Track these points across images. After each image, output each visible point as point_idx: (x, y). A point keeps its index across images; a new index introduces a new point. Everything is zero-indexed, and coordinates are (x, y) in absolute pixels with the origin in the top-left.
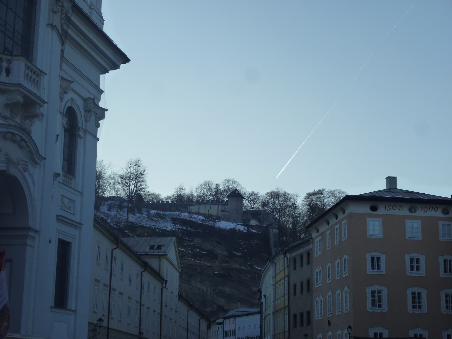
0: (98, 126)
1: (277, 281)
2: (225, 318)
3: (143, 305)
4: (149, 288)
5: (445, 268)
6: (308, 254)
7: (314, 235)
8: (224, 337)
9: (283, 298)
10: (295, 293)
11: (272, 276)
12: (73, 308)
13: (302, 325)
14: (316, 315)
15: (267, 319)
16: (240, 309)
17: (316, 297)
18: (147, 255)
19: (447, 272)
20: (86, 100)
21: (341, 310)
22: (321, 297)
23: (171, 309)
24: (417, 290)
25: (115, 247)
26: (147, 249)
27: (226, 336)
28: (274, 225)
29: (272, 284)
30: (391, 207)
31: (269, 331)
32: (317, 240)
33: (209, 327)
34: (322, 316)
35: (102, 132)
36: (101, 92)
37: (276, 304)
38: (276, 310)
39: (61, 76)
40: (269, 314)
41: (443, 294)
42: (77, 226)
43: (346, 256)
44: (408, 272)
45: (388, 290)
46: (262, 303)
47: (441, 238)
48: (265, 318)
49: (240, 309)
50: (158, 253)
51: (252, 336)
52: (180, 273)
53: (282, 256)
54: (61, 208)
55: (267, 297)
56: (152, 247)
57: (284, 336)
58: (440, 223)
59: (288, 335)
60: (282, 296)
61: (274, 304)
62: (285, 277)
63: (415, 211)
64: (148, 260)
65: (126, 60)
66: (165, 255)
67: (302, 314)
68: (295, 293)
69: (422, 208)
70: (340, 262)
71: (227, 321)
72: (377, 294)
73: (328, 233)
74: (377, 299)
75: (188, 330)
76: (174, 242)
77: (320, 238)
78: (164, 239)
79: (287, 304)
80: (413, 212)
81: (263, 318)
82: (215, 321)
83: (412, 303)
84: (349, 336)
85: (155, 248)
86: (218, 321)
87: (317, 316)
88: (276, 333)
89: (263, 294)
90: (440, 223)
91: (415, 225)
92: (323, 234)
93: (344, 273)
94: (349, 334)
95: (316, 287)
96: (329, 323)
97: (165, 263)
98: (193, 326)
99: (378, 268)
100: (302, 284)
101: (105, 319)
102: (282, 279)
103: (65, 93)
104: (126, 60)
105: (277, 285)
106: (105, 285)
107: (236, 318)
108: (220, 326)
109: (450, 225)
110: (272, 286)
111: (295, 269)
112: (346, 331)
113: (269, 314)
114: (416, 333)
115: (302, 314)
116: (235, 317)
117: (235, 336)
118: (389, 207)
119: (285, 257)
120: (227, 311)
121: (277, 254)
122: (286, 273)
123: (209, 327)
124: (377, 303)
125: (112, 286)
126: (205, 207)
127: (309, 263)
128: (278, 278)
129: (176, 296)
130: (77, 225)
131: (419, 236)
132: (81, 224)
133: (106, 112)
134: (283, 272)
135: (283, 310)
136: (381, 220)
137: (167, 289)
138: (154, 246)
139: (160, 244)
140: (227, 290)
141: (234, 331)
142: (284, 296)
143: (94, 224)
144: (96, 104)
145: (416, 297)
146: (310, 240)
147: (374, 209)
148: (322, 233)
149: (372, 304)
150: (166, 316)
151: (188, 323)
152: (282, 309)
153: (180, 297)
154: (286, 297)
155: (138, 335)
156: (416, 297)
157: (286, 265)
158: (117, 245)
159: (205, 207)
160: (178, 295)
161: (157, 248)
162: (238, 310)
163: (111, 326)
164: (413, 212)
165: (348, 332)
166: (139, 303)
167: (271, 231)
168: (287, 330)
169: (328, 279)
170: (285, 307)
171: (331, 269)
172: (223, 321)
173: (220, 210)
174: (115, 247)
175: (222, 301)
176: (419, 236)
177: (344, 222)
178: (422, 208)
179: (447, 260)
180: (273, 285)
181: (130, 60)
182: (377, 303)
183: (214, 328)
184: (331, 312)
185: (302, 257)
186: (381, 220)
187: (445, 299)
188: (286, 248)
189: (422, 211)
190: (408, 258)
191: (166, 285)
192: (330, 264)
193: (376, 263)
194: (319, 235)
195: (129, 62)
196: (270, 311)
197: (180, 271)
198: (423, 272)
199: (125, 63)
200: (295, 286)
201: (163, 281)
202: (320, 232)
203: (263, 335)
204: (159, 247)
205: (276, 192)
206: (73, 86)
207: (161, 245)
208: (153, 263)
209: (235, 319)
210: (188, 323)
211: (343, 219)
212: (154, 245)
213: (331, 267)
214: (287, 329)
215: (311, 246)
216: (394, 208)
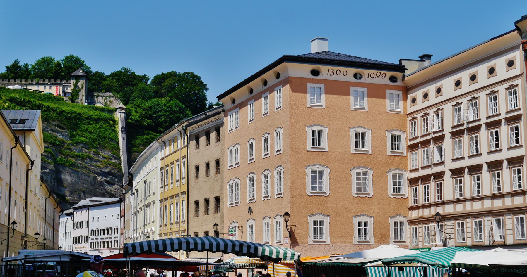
2: (75, 209)
5: (356, 142)
8: (74, 228)
10: (197, 177)
19: (359, 147)
27: (77, 228)
29: (160, 167)
51: (108, 228)
68: (197, 177)
80: (358, 78)
83: (312, 178)
85: (17, 122)
100: (208, 165)
108: (69, 218)
114: (315, 219)
117: (88, 228)
118: (332, 71)
138: (17, 120)
141: (87, 222)
149: (314, 236)
164: (358, 78)
187: (392, 180)
189: (368, 77)
191: (32, 167)
204: (23, 121)
212: (15, 118)
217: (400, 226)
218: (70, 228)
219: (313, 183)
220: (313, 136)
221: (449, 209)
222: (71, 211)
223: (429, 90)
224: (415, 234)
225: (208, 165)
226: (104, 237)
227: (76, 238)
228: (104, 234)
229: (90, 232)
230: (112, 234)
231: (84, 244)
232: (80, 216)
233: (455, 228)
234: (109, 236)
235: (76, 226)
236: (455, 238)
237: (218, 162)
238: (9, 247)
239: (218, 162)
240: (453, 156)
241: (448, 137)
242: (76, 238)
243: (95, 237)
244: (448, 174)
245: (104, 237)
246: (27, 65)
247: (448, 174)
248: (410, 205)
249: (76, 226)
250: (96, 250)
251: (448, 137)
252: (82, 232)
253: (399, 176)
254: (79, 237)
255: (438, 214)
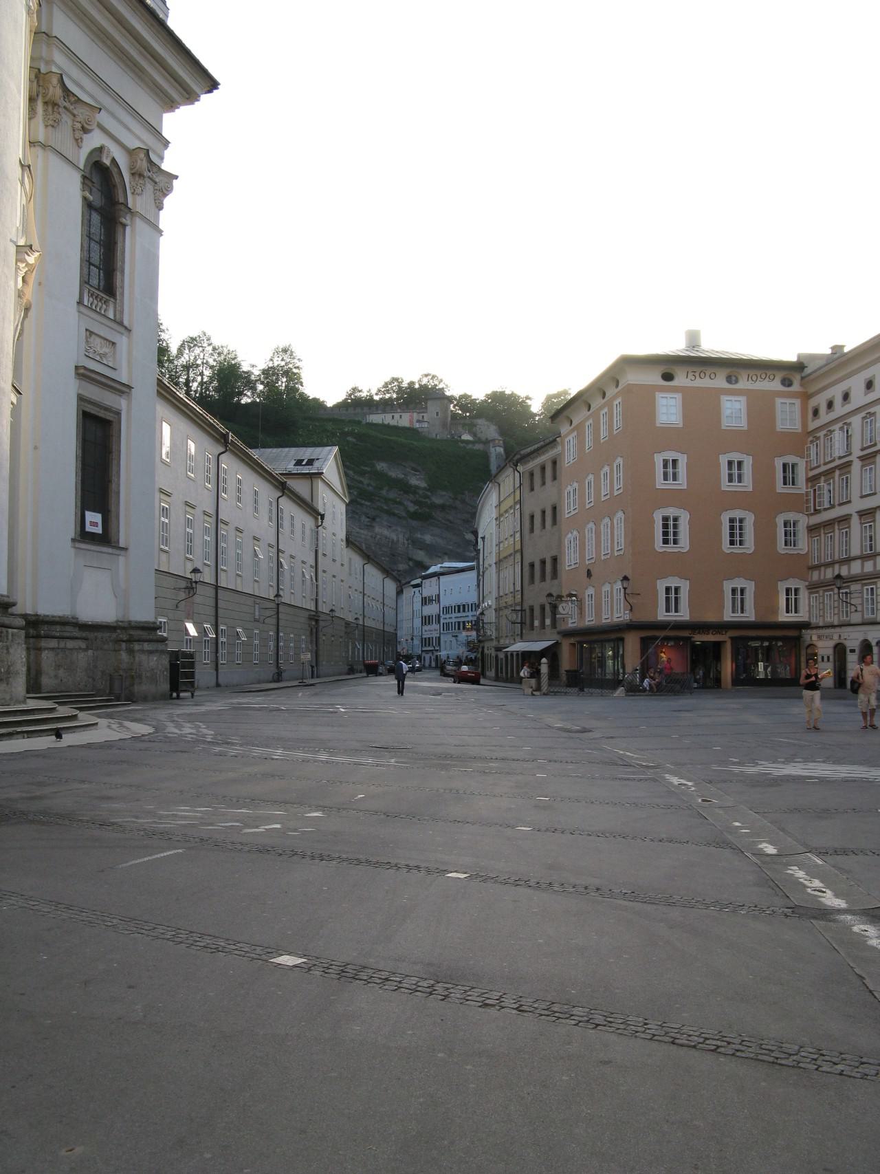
0: (160, 207)
1: (502, 512)
3: (283, 552)
4: (292, 525)
5: (785, 478)
6: (554, 463)
7: (565, 429)
9: (512, 539)
10: (532, 530)
11: (494, 505)
12: (122, 545)
13: (543, 578)
14: (567, 561)
15: (487, 573)
16: (447, 564)
17: (567, 534)
18: (290, 475)
20: (131, 153)
21: (609, 551)
22: (575, 533)
23: (334, 560)
24: (737, 514)
25: (222, 450)
26: (291, 467)
28: (497, 441)
29: (495, 517)
30: (697, 375)
31: (490, 592)
32: (570, 437)
33: (400, 592)
34: (576, 563)
35: (166, 219)
36: (166, 143)
37: (501, 549)
38: (501, 557)
39: (98, 122)
40: (490, 566)
41: (780, 520)
42: (123, 392)
43: (620, 460)
44: (725, 485)
45: (690, 515)
46: (479, 550)
47: (780, 427)
48: (483, 573)
49: (447, 564)
50: (308, 472)
52: (347, 505)
53: (509, 471)
54: (86, 355)
55: (486, 540)
56: (299, 463)
57: (515, 597)
58: (779, 401)
59: (520, 596)
60: (511, 536)
61: (497, 548)
62: (515, 503)
63: (737, 382)
64: (291, 483)
65: (213, 85)
66: (319, 474)
67: (543, 562)
68: (532, 530)
69: (749, 375)
70: (608, 472)
71: (427, 582)
72: (671, 523)
73: (588, 423)
74: (671, 530)
75: (384, 604)
76: (335, 455)
77: (575, 433)
78: (319, 449)
79: (518, 547)
80: (734, 382)
81: (481, 573)
82: (409, 582)
83: (730, 537)
84: (625, 593)
85: (304, 463)
86: (414, 582)
87: (570, 560)
88: (501, 594)
89: (480, 535)
90: (779, 401)
91: (737, 406)
92: (580, 428)
93: (616, 488)
94: (625, 589)
95: (567, 516)
96: (589, 574)
97: (320, 486)
98: (373, 588)
99: (675, 478)
100: (544, 512)
101: (361, 618)
102: (511, 507)
103: (85, 131)
104: (213, 85)
105: (502, 519)
106: (270, 545)
107: (441, 577)
108: (416, 590)
109: (794, 404)
110: (494, 521)
111: (532, 489)
112: (619, 585)
113: (490, 566)
115: (543, 562)
116: (437, 575)
119: (516, 472)
120: (427, 568)
121: (501, 469)
122: (518, 498)
123: (400, 592)
124: (671, 537)
125: (220, 517)
126: (393, 417)
127: (555, 478)
128: (504, 507)
129: (342, 540)
130: (123, 389)
131: (743, 424)
132: (130, 387)
133: (174, 181)
134: (512, 496)
135: (512, 557)
136: (679, 396)
137: (324, 528)
139: (312, 458)
140: (428, 538)
142: (513, 535)
143: (157, 390)
144: (152, 162)
145: (736, 527)
146: (558, 439)
147: (668, 377)
148: (577, 425)
150: (324, 571)
151: (384, 595)
152: (510, 555)
153: (349, 542)
154: (518, 535)
155: (273, 599)
156: (736, 527)
157: (517, 485)
158: (226, 446)
159: (393, 417)
160: (344, 538)
161: (306, 465)
162: (443, 565)
163: (222, 583)
164: (734, 382)
165: (623, 585)
166: (275, 548)
167: (492, 450)
168: (520, 589)
169: (588, 502)
170: (516, 552)
171: (592, 483)
172: (422, 582)
173: (415, 421)
174: (222, 450)
175: (420, 555)
176: (743, 424)
177: (616, 402)
178: (749, 375)
179: (788, 464)
180: (496, 519)
181: (219, 84)
182: (671, 537)
183: (408, 592)
184: (592, 555)
185: (543, 468)
186: (679, 396)
187: (783, 530)
188: (518, 457)
190: (723, 460)
191: (322, 522)
192: (591, 477)
193: (670, 470)
194: (573, 431)
195: (217, 88)
196: (491, 559)
197: (347, 502)
198: (748, 484)
199: (210, 91)
200: (532, 517)
201: (318, 516)
202: (575, 423)
203: (481, 599)
204: (310, 462)
205: (500, 392)
206: (103, 118)
207: (314, 459)
208: (300, 487)
209: (439, 578)
210: (384, 595)
211: (614, 398)
213: (592, 480)
214: (518, 587)
215: (558, 449)
216: (702, 375)
217: (796, 595)
218: (418, 605)
219: (732, 535)
220: (784, 471)
221: (856, 568)
222: (418, 581)
223: (866, 394)
224: (739, 599)
225: (544, 512)
226: (459, 615)
227: (425, 617)
228: (459, 611)
229: (442, 610)
230: (468, 611)
231: (435, 626)
232: (429, 588)
233: (862, 597)
234: (464, 614)
235: (426, 601)
236: (862, 611)
237: (554, 509)
238: (219, 618)
239: (554, 509)
240: (861, 492)
241: (856, 465)
242: (425, 617)
243: (448, 616)
244: (855, 520)
245: (459, 615)
246: (412, 383)
247: (855, 520)
248: (810, 564)
249: (426, 601)
250: (448, 633)
251: (856, 465)
252: (432, 610)
253: (794, 524)
254: (429, 617)
255: (839, 577)
